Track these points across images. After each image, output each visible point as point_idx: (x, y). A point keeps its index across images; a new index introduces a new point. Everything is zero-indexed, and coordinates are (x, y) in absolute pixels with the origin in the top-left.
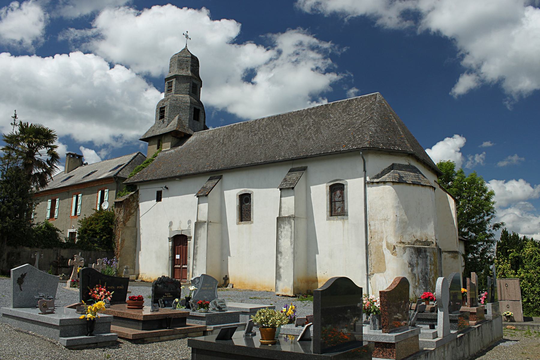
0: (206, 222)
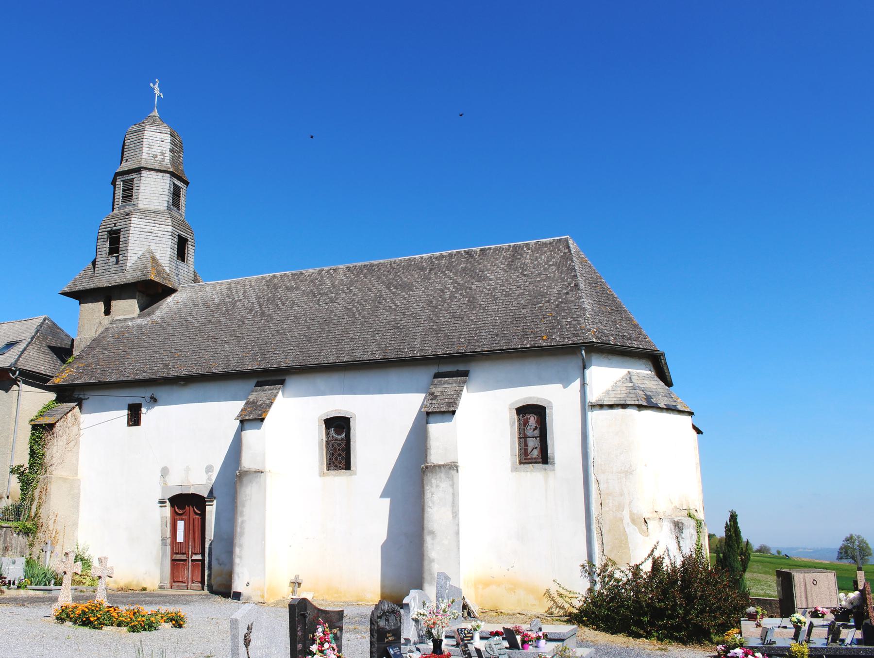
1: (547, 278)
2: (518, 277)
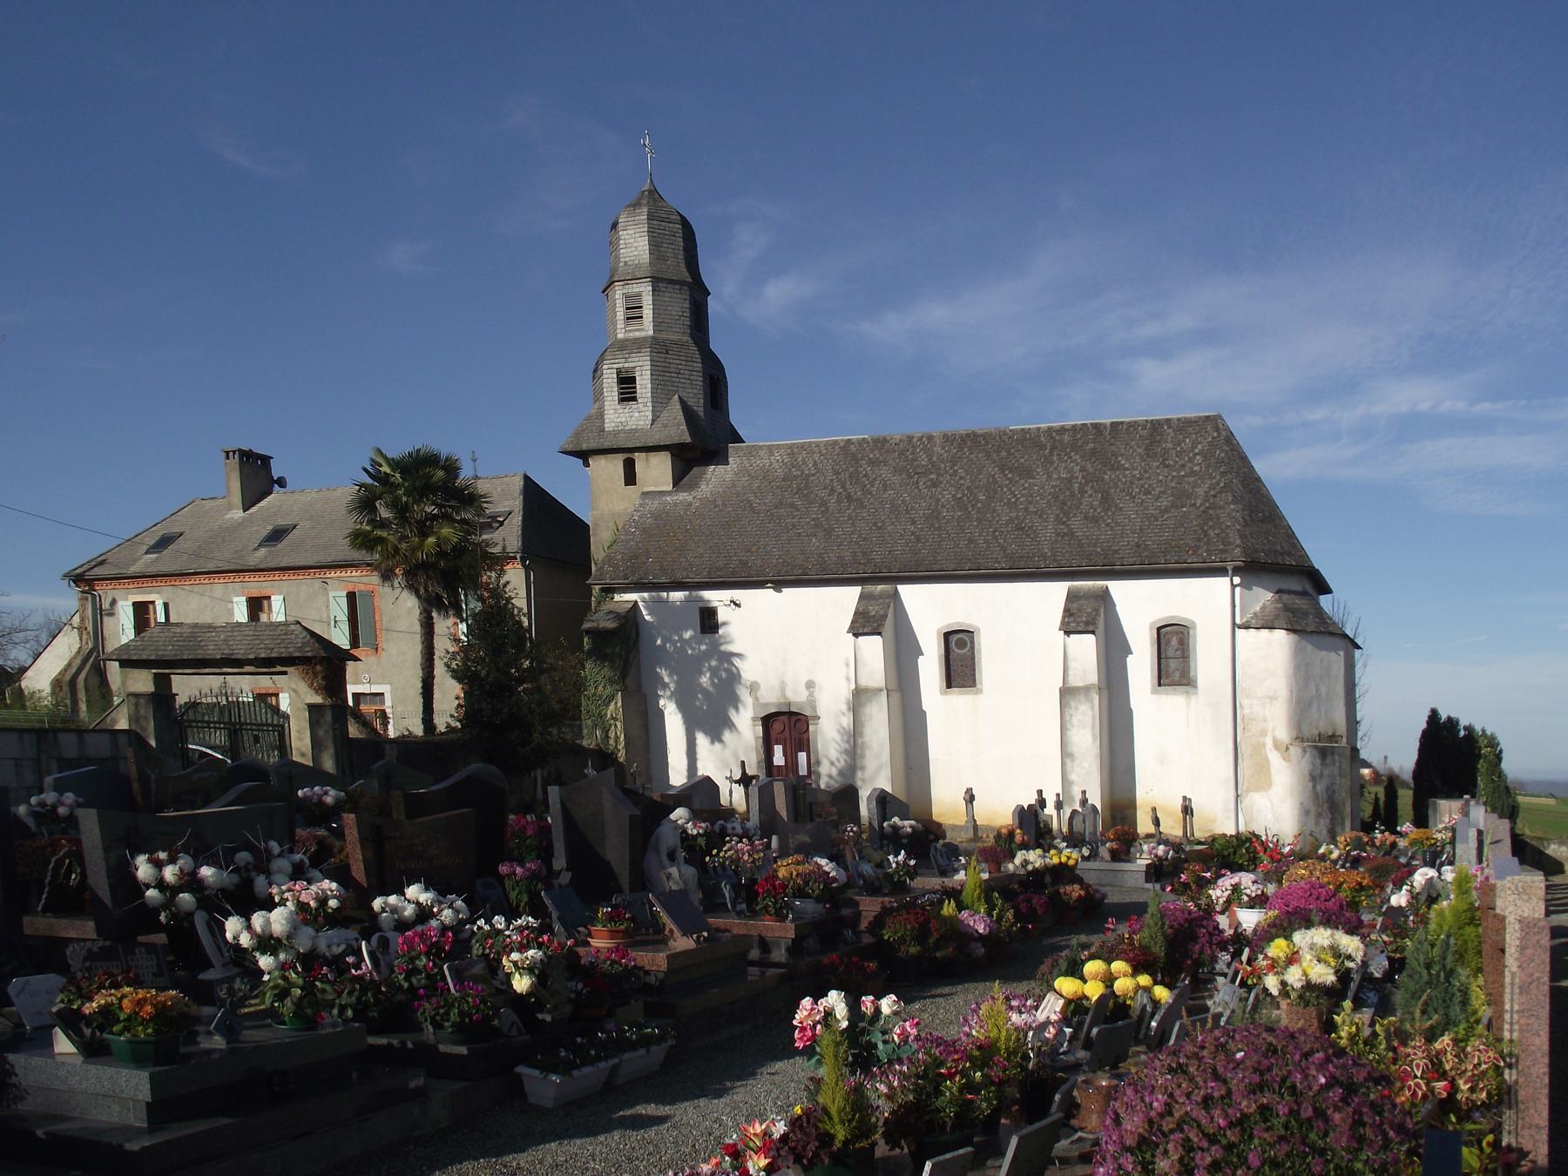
0: (881, 690)
1: (1193, 473)
2: (1158, 467)
